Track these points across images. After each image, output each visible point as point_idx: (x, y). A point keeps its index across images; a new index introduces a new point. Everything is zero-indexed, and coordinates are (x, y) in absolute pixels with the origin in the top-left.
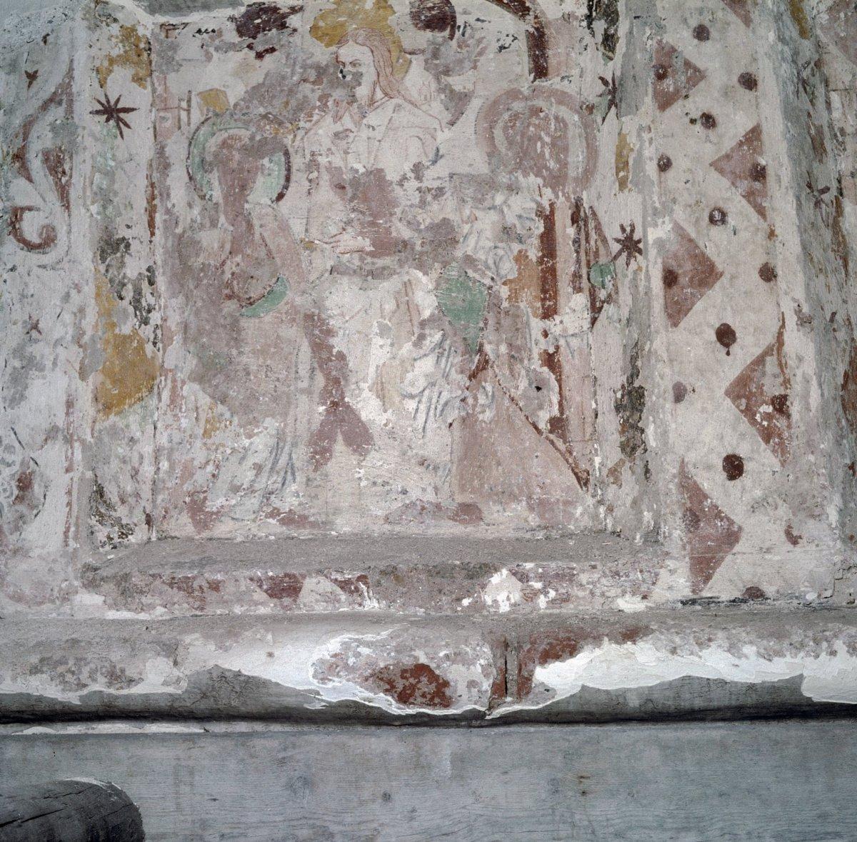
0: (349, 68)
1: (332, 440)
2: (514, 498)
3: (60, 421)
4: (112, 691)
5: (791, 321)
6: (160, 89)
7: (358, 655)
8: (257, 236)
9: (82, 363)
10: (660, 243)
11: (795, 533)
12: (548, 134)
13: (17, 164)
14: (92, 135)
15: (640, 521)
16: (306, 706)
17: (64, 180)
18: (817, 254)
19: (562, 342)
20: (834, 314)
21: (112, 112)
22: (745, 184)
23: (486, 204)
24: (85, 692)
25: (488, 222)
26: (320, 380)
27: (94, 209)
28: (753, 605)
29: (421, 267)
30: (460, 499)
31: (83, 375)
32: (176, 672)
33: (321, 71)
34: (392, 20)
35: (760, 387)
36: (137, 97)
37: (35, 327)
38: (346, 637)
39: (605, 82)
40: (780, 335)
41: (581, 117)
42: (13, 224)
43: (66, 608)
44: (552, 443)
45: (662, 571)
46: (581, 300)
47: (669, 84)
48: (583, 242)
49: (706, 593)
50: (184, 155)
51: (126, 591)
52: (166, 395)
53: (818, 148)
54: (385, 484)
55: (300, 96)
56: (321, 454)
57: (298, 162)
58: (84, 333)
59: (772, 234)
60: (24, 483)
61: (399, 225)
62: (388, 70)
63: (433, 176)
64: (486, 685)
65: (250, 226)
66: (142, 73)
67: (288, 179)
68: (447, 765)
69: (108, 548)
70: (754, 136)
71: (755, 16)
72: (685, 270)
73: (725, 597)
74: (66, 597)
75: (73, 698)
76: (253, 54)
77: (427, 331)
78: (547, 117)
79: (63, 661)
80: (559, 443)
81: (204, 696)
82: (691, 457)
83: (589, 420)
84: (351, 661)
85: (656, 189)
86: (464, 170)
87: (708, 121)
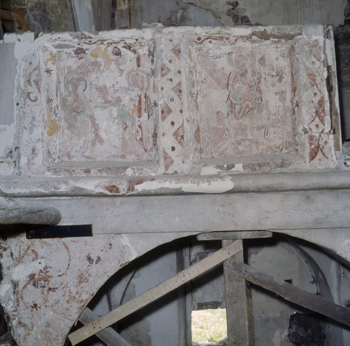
0: (98, 63)
1: (96, 141)
2: (132, 154)
3: (41, 138)
4: (55, 190)
5: (185, 121)
6: (58, 65)
7: (102, 184)
8: (80, 98)
9: (45, 126)
10: (161, 105)
11: (184, 161)
12: (140, 79)
13: (28, 83)
14: (44, 77)
15: (156, 159)
16: (92, 193)
17: (39, 87)
18: (191, 107)
19: (142, 123)
20: (194, 119)
21: (48, 71)
22: (178, 93)
23: (128, 93)
24: (49, 191)
25: (127, 97)
26: (93, 129)
27: (46, 93)
28: (176, 175)
29: (114, 106)
30: (122, 154)
31: (45, 128)
32: (67, 187)
33: (93, 63)
34: (108, 53)
35: (179, 134)
36: (53, 67)
37: (34, 118)
38: (100, 180)
39: (152, 70)
40: (183, 123)
41: (147, 76)
42: (28, 96)
43: (44, 175)
44: (140, 143)
45: (159, 168)
46: (146, 114)
47: (164, 72)
48: (147, 102)
49: (167, 172)
50: (63, 80)
51: (56, 172)
52: (61, 132)
53: (193, 85)
54: (107, 151)
55: (88, 68)
56: (94, 144)
57: (88, 83)
58: (44, 120)
59: (182, 104)
60: (34, 150)
61: (110, 97)
62: (107, 64)
63: (117, 87)
64: (126, 189)
65: (78, 96)
66: (54, 62)
67: (86, 86)
68: (119, 203)
69: (51, 163)
70: (180, 83)
71: (181, 58)
72: (165, 110)
73: (171, 173)
74: (44, 173)
75: (47, 192)
76: (78, 59)
77: (115, 120)
78: (140, 75)
79: (45, 185)
80: (141, 143)
81: (73, 191)
82: (165, 147)
83: (147, 138)
84: (101, 185)
85: (160, 94)
86: (123, 86)
87: (171, 80)
